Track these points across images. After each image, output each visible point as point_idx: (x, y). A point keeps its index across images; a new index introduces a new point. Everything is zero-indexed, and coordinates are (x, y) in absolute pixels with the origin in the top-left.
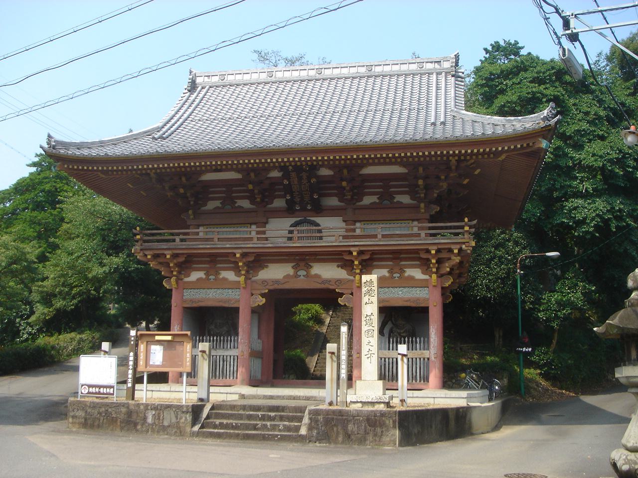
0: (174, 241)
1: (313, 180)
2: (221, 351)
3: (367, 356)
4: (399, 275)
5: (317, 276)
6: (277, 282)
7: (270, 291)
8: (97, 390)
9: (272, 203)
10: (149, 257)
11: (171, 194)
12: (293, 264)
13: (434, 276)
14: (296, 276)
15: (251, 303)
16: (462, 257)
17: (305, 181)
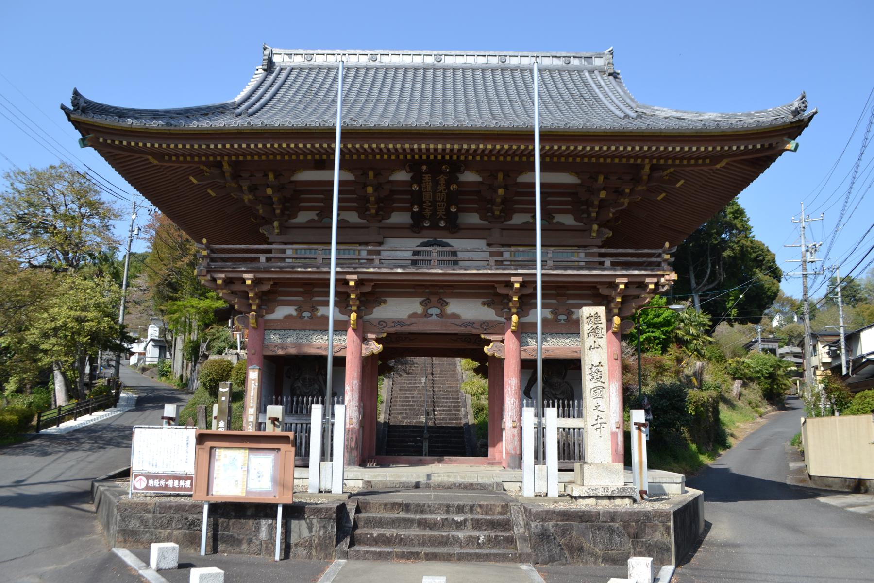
0: (257, 260)
1: (453, 187)
4: (565, 317)
5: (455, 316)
6: (400, 323)
7: (389, 334)
8: (163, 482)
9: (389, 217)
11: (250, 197)
12: (421, 299)
14: (426, 315)
17: (441, 188)
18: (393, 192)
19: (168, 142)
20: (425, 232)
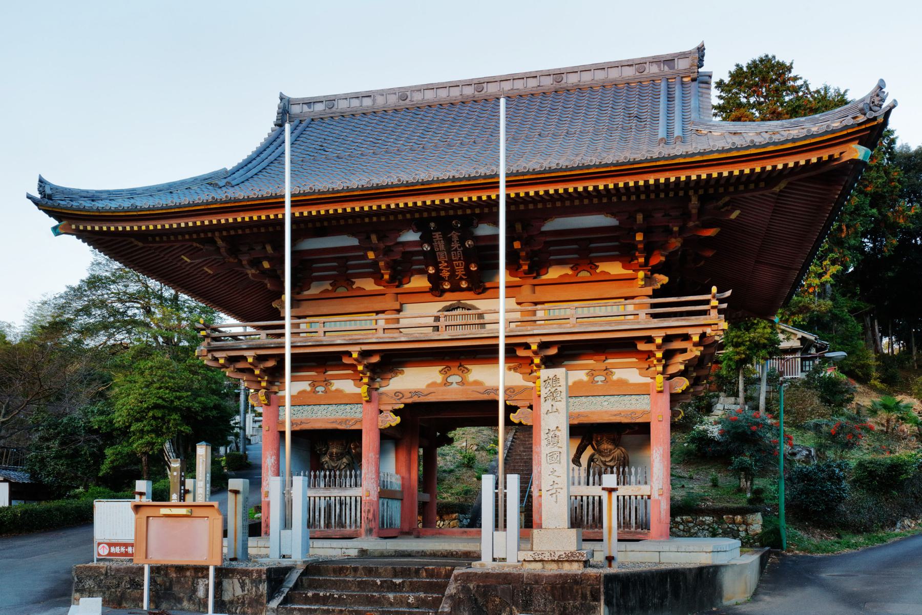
1: (469, 243)
2: (336, 491)
3: (550, 492)
4: (603, 378)
5: (477, 383)
6: (417, 393)
10: (222, 361)
11: (253, 271)
12: (441, 368)
13: (660, 378)
14: (446, 383)
15: (380, 424)
16: (705, 347)
17: (456, 245)
18: (405, 254)
19: (116, 225)
20: (447, 295)
